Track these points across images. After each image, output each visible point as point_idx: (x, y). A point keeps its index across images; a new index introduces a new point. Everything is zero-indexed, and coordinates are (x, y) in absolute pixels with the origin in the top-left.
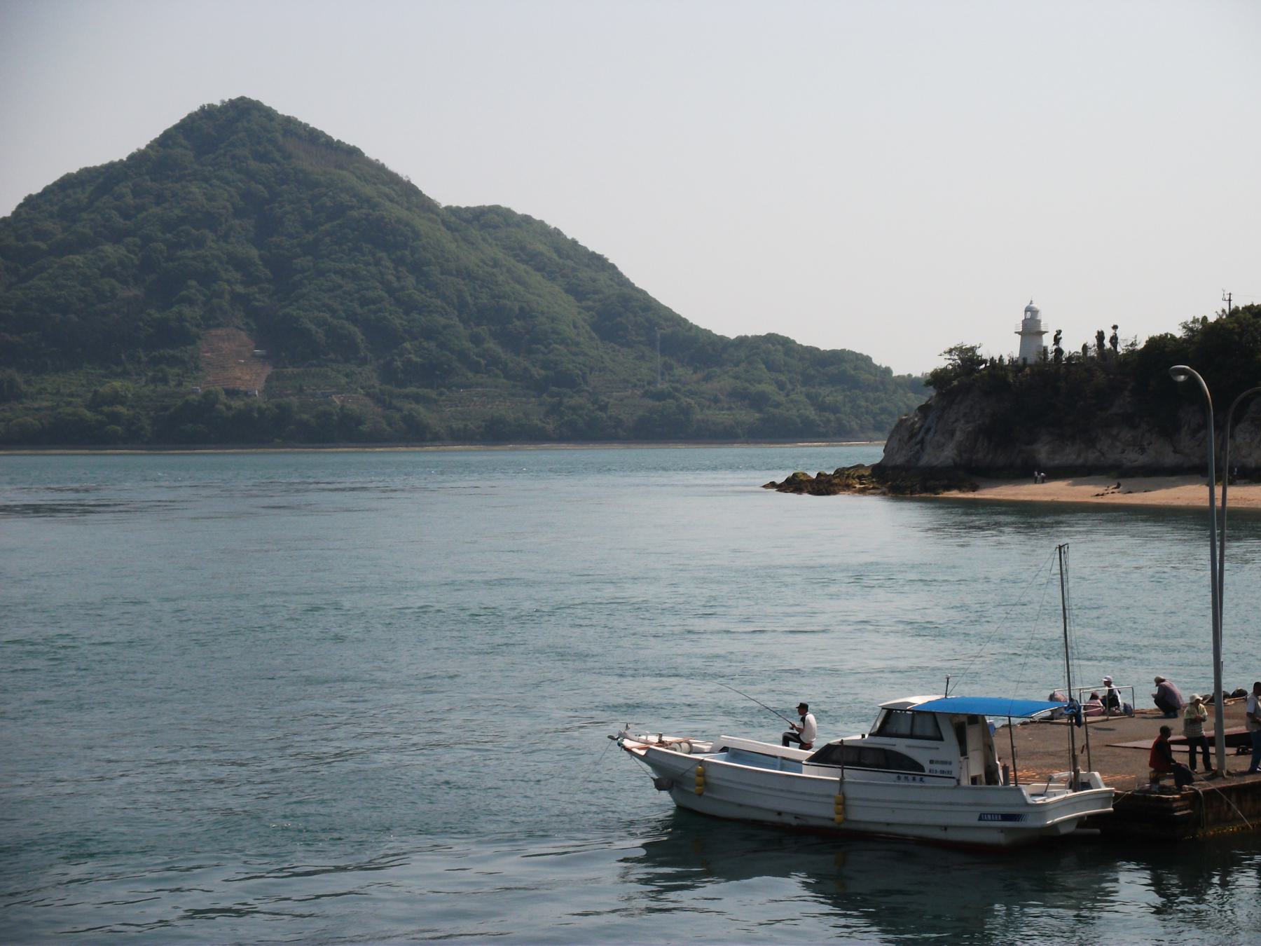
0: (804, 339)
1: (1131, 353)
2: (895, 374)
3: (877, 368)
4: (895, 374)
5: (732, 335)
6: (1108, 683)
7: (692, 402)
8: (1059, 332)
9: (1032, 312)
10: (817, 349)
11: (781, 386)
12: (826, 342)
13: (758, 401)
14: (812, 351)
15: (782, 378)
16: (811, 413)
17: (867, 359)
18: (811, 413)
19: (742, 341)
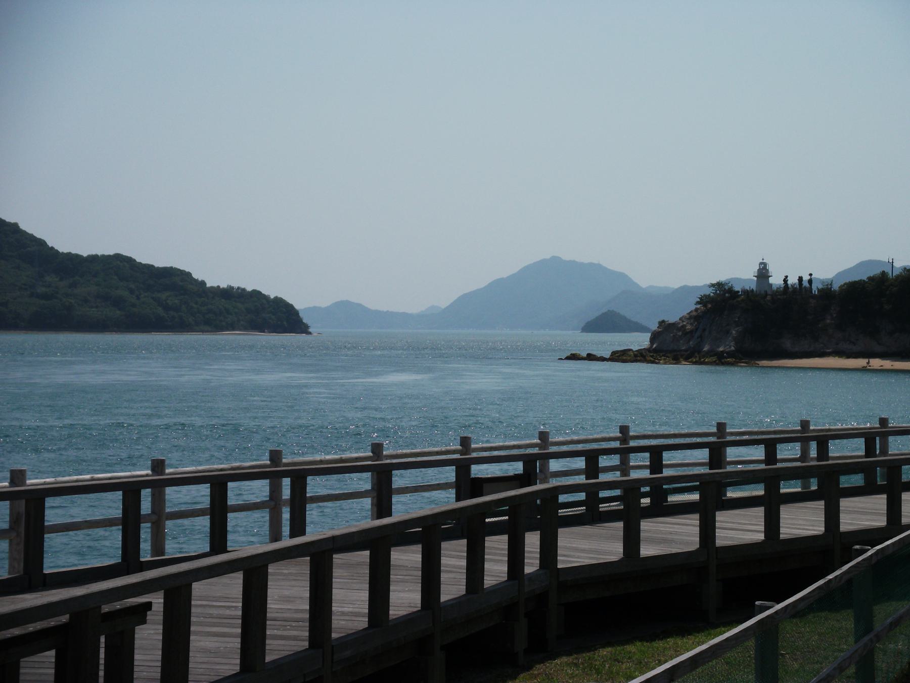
0: (143, 257)
1: (898, 277)
2: (208, 285)
3: (196, 281)
4: (208, 285)
5: (85, 255)
6: (811, 275)
7: (73, 301)
8: (787, 277)
9: (787, 277)
10: (153, 266)
11: (132, 292)
12: (160, 261)
13: (118, 303)
14: (150, 267)
15: (132, 286)
16: (160, 311)
17: (189, 274)
18: (160, 311)
19: (93, 259)
